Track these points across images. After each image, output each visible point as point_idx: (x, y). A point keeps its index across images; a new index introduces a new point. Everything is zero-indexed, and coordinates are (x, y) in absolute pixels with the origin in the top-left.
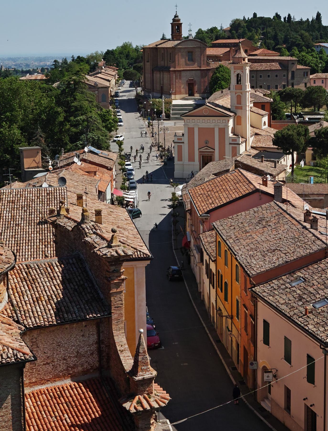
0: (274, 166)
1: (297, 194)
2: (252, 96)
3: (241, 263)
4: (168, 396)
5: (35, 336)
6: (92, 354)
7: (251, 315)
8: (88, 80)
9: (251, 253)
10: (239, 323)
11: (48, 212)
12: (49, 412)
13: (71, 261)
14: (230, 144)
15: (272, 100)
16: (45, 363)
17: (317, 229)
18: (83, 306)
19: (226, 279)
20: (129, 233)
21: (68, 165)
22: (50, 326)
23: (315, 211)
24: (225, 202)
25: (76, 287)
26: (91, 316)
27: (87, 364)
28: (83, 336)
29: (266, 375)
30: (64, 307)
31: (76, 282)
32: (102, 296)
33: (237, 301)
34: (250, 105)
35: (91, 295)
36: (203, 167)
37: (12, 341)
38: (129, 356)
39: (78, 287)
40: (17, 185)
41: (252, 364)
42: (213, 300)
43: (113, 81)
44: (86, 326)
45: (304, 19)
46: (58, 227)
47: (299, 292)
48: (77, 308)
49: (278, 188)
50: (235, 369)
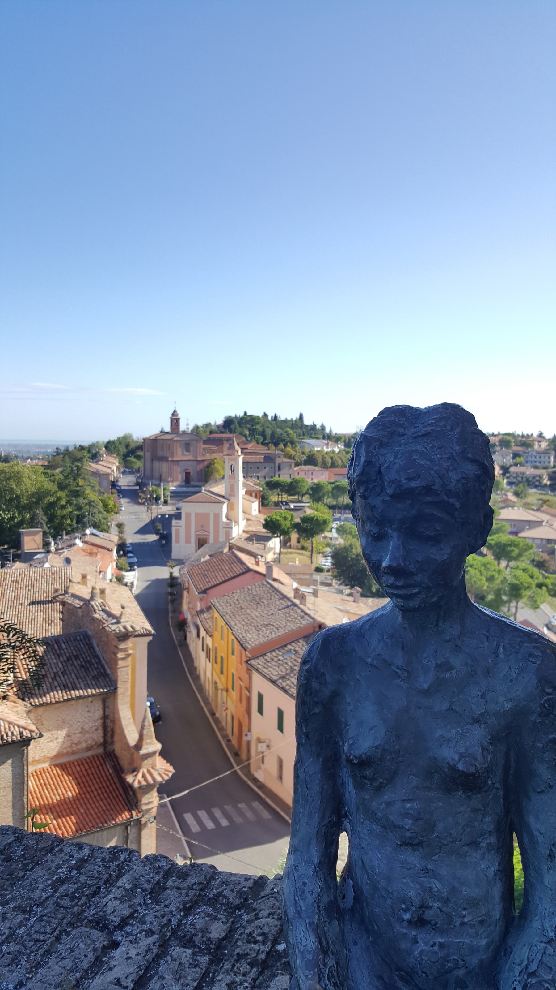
0: (263, 548)
1: (287, 574)
2: (245, 485)
3: (237, 637)
4: (171, 769)
5: (40, 713)
6: (96, 730)
7: (246, 688)
8: (91, 466)
9: (246, 628)
10: (234, 695)
11: (53, 591)
12: (52, 790)
13: (78, 638)
14: (224, 528)
15: (261, 489)
16: (49, 740)
17: (305, 605)
18: (89, 682)
19: (222, 653)
20: (132, 610)
21: (70, 546)
22: (57, 702)
23: (303, 589)
24: (221, 581)
25: (83, 663)
26: (97, 691)
27: (91, 740)
28: (88, 711)
29: (260, 745)
30: (71, 683)
31: (83, 658)
32: (108, 671)
33: (233, 675)
34: (242, 492)
35: (98, 671)
36: (199, 549)
37: (17, 719)
38: (133, 730)
39: (85, 663)
40: (18, 565)
41: (246, 735)
42: (209, 674)
43: (115, 468)
44: (92, 702)
45: (289, 419)
46: (66, 604)
47: (290, 664)
48: (84, 684)
49: (269, 568)
50: (229, 741)
